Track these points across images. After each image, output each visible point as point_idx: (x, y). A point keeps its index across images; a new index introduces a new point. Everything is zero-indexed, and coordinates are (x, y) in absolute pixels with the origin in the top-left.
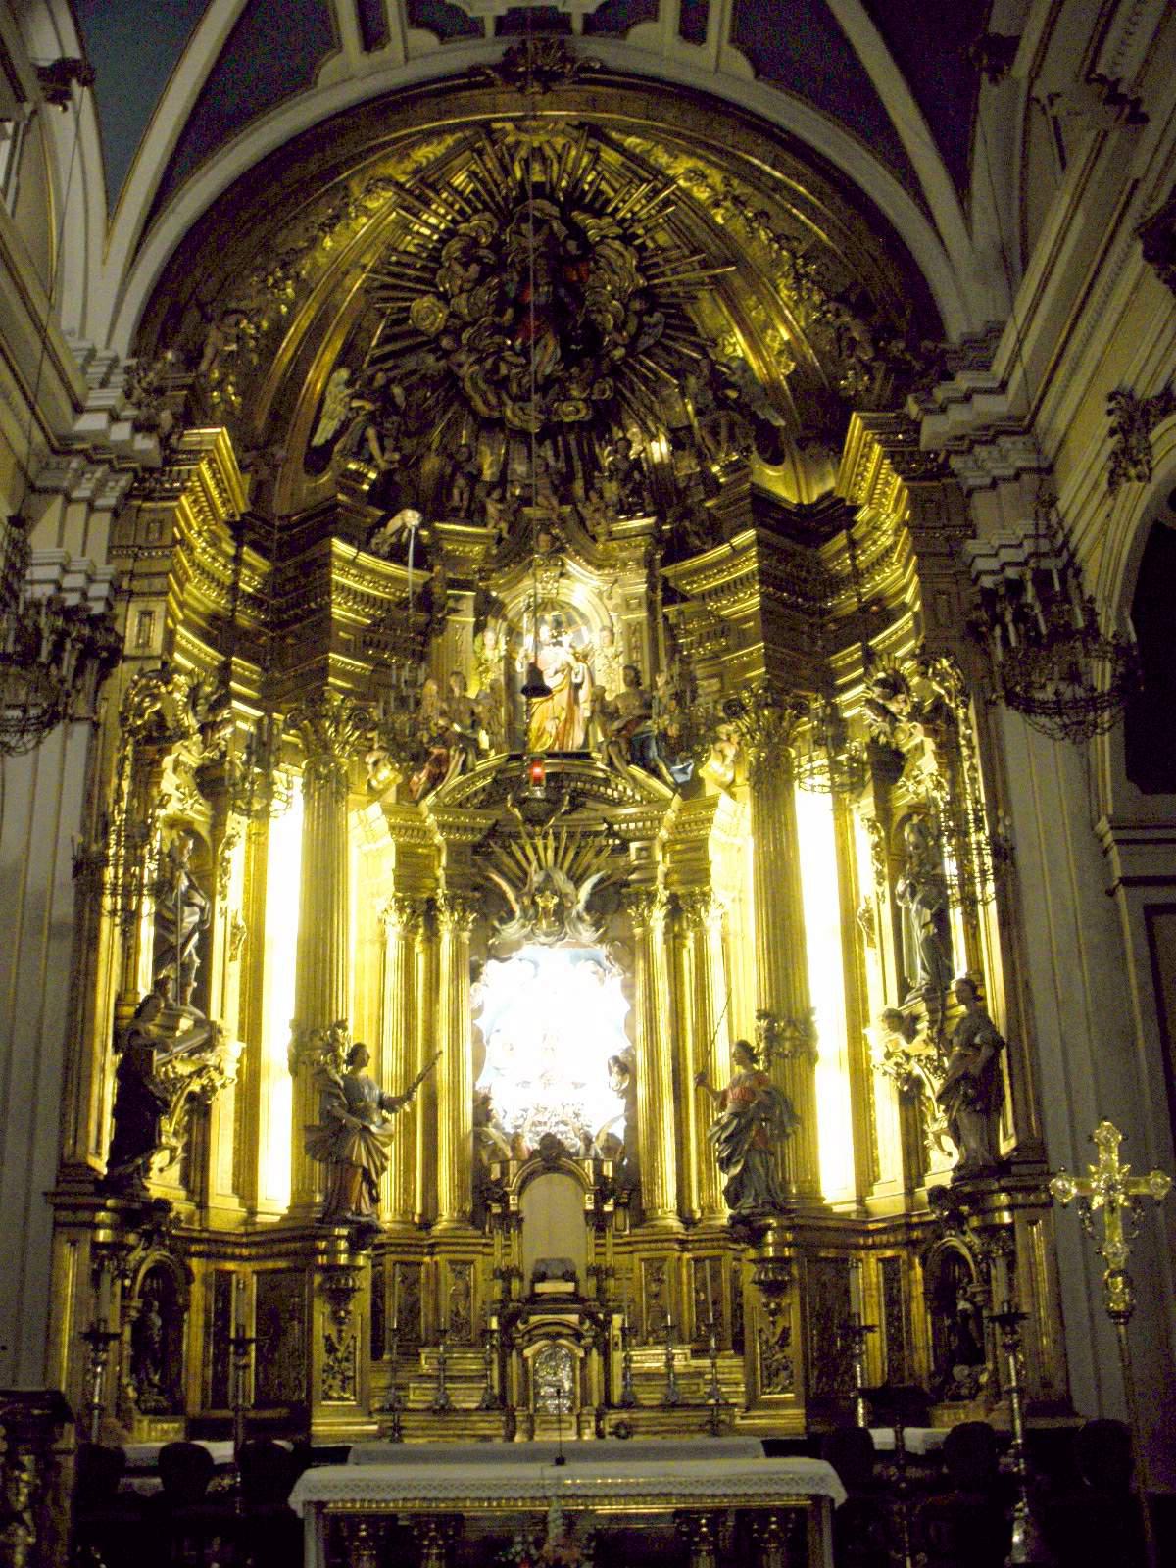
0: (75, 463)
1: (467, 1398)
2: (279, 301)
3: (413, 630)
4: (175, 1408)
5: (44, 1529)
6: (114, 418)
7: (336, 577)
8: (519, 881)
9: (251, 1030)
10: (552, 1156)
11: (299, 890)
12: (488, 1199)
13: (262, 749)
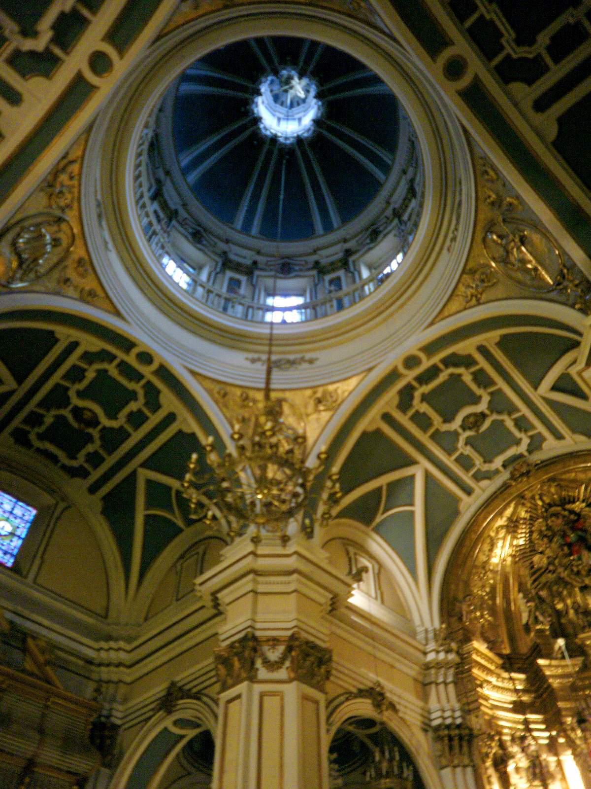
0: (433, 671)
2: (488, 579)
6: (438, 652)
7: (548, 673)
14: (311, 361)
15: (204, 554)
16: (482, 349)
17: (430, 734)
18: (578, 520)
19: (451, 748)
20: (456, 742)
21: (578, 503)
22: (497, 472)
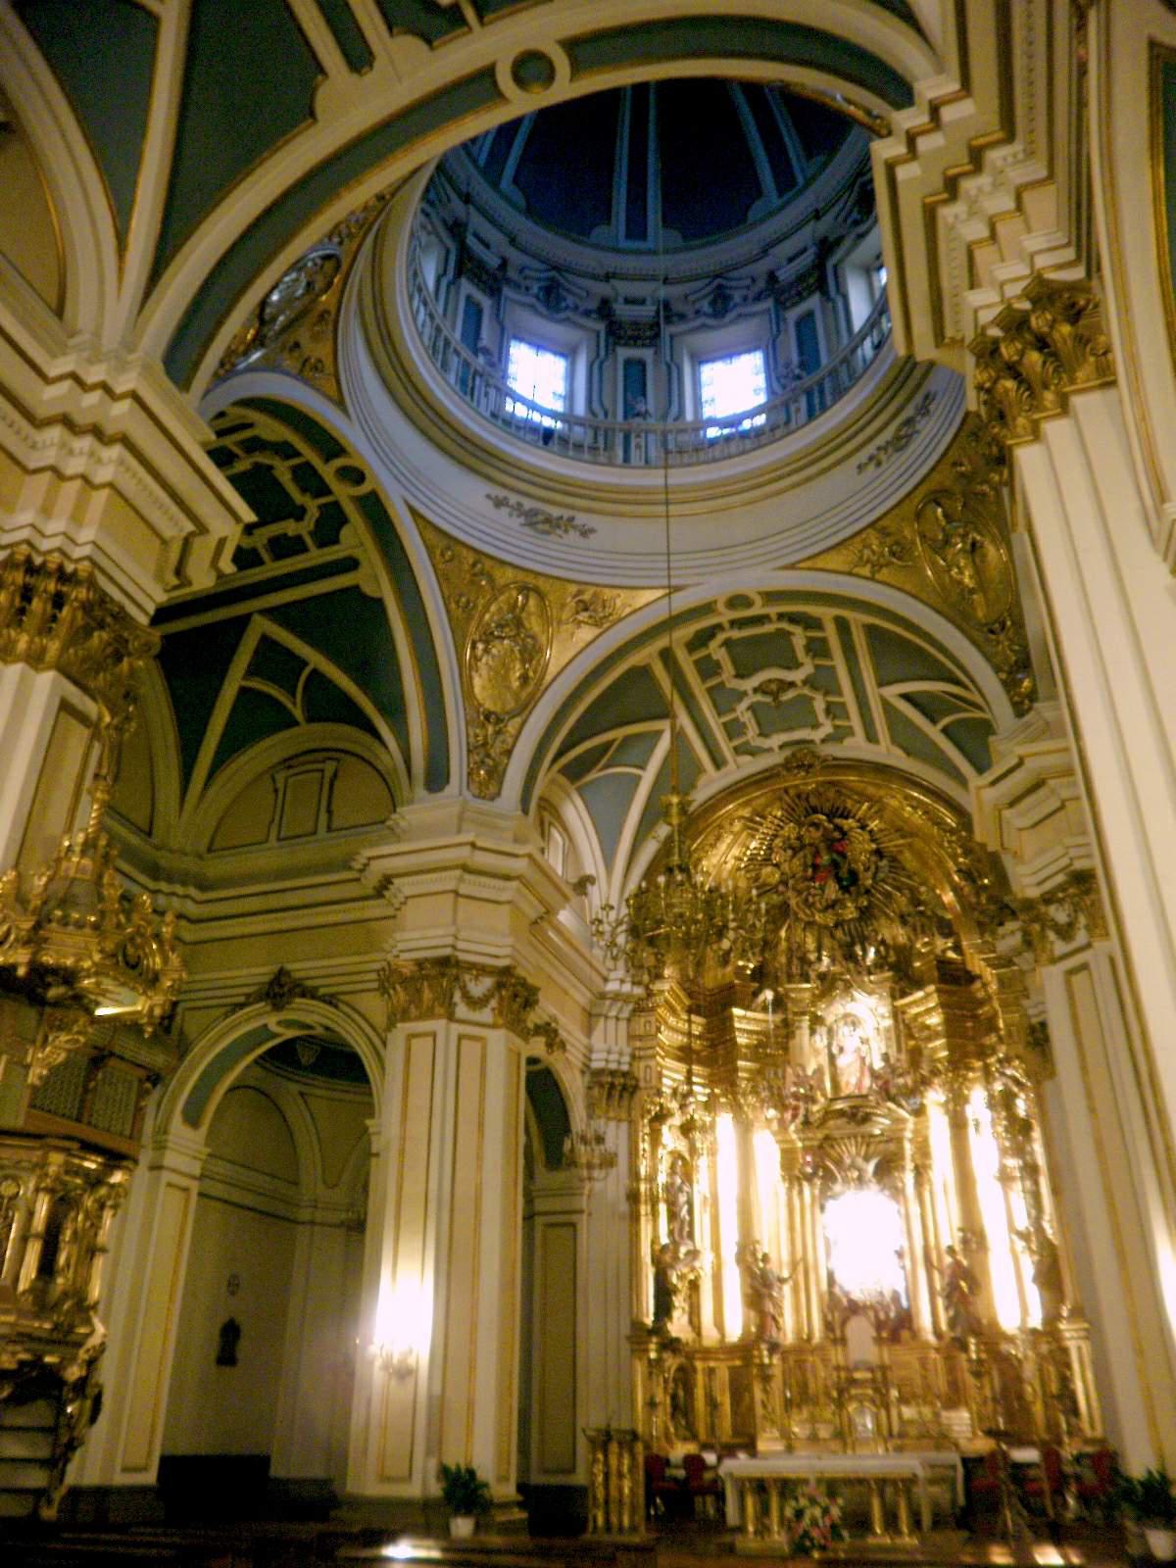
0: (608, 1002)
1: (824, 1432)
3: (777, 1047)
4: (694, 1437)
5: (634, 1481)
6: (622, 981)
7: (737, 1025)
9: (716, 1247)
12: (835, 1333)
13: (710, 1106)
14: (585, 533)
15: (335, 775)
16: (842, 625)
17: (587, 1078)
18: (839, 840)
19: (610, 1096)
20: (616, 1094)
21: (850, 821)
22: (770, 750)
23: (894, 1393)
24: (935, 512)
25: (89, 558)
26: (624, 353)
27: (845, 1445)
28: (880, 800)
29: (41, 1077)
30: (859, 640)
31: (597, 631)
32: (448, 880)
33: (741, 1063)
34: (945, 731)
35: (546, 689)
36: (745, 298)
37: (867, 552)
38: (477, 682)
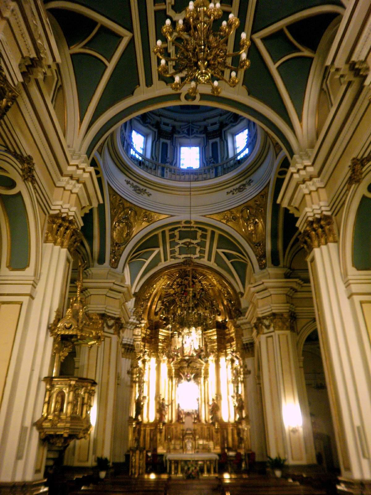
1: (178, 447)
3: (169, 339)
6: (134, 319)
8: (184, 374)
10: (188, 414)
11: (154, 373)
14: (149, 195)
16: (213, 233)
17: (122, 346)
19: (127, 351)
20: (129, 351)
22: (180, 258)
23: (197, 437)
24: (247, 212)
25: (74, 216)
26: (162, 140)
27: (183, 451)
28: (206, 276)
29: (63, 360)
30: (216, 237)
31: (148, 224)
32: (104, 292)
33: (160, 344)
34: (232, 263)
35: (133, 237)
36: (197, 132)
37: (226, 217)
38: (115, 233)
